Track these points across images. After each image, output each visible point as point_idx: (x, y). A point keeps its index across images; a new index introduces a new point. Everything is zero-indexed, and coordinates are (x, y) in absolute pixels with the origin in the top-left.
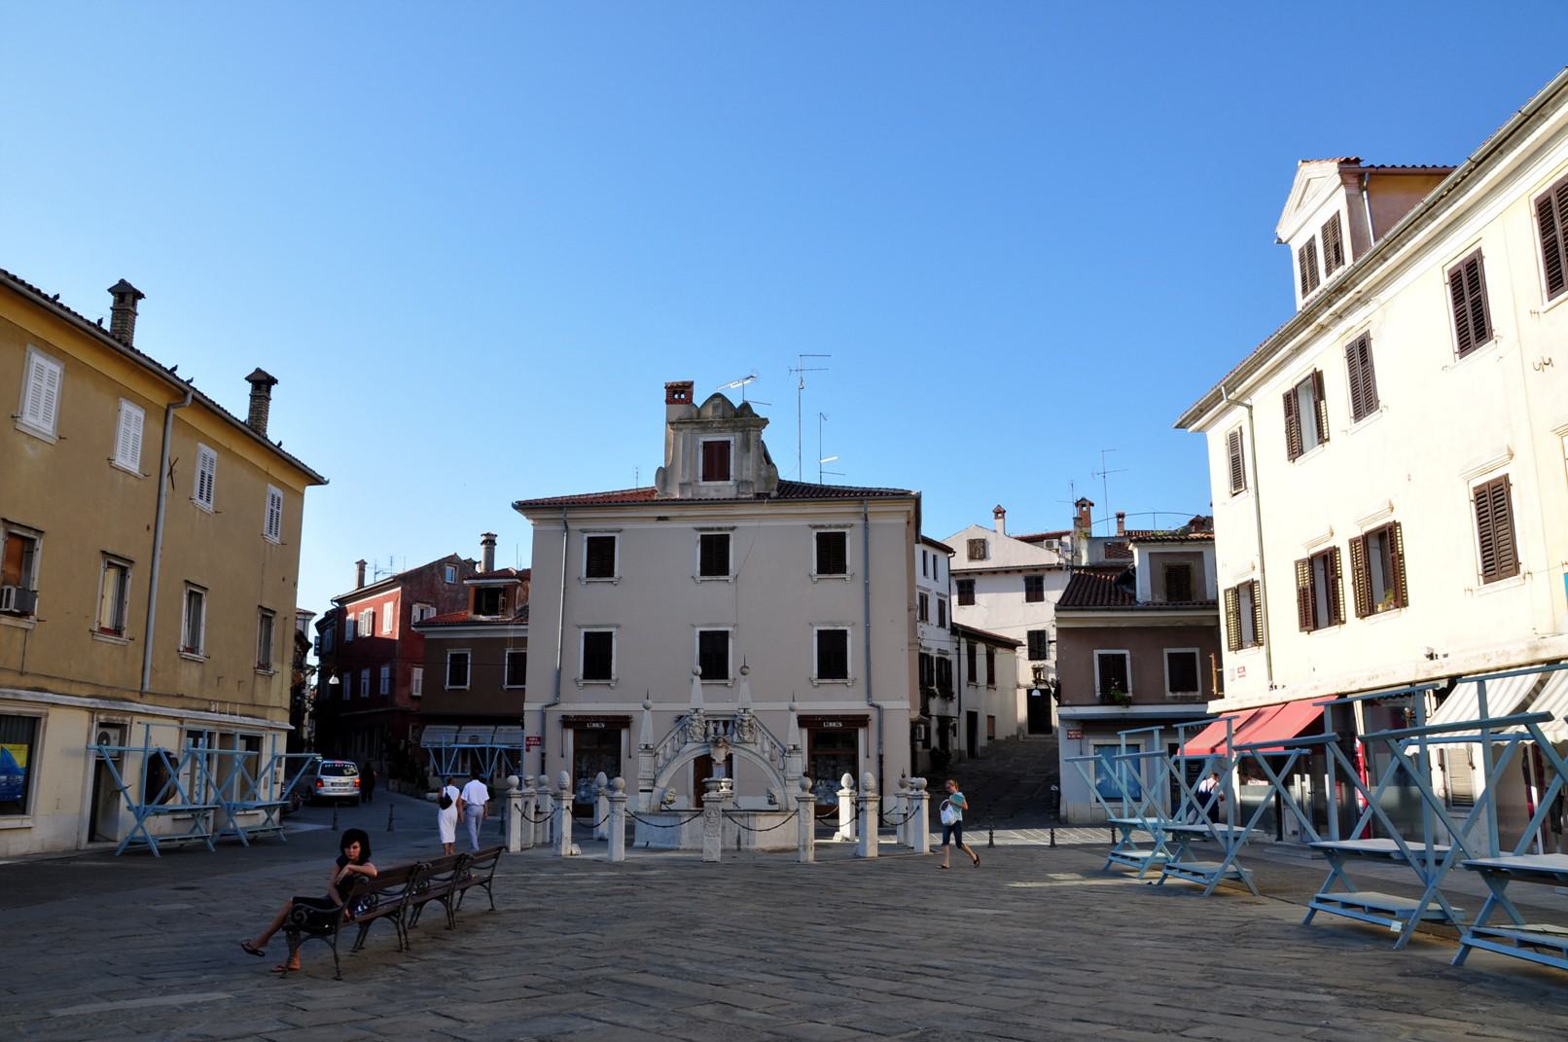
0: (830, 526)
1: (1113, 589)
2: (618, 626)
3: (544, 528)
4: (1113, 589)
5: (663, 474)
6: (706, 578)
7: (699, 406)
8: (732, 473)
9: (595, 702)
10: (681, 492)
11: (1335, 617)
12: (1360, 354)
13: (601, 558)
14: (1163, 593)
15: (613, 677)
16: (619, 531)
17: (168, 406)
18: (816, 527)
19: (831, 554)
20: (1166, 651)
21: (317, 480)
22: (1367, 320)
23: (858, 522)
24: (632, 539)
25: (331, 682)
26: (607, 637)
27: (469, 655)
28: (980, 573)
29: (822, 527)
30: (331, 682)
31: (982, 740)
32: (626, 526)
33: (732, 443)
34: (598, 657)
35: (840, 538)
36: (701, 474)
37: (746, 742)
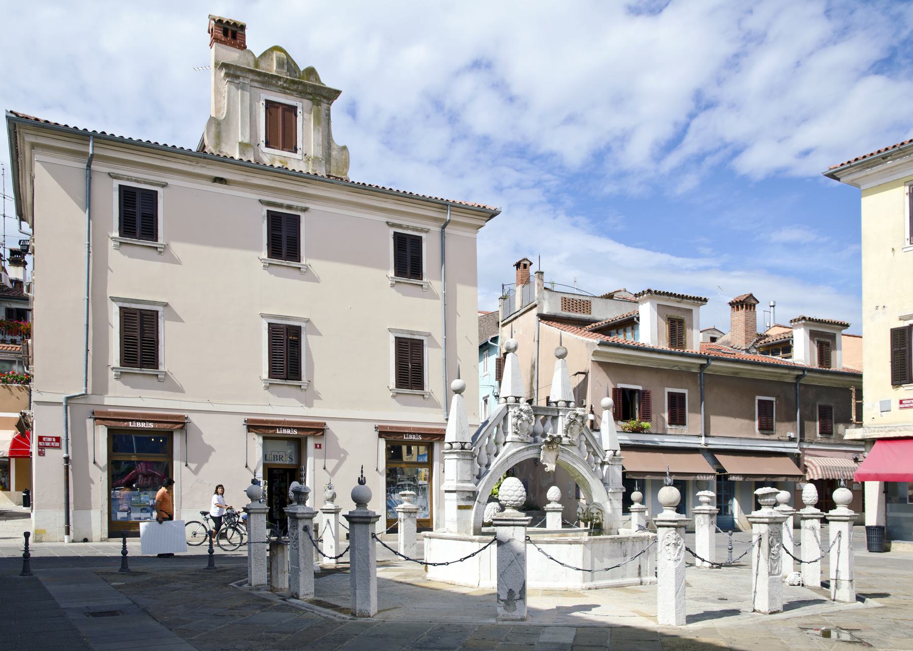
0: (408, 228)
2: (166, 305)
5: (218, 126)
10: (242, 152)
16: (164, 185)
18: (393, 225)
20: (758, 398)
23: (435, 228)
25: (343, 455)
26: (296, 332)
29: (400, 226)
30: (343, 455)
32: (173, 181)
35: (418, 241)
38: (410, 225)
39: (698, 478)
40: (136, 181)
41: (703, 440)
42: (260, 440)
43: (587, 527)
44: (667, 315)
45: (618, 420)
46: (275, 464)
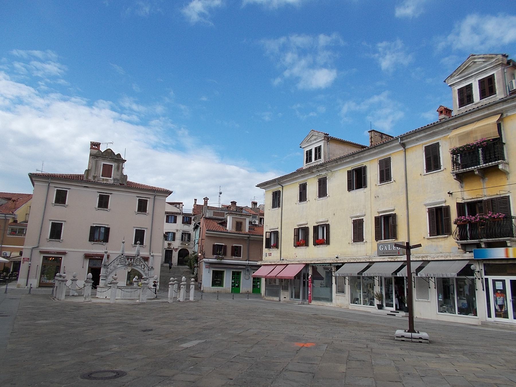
0: (143, 197)
2: (65, 221)
5: (88, 171)
6: (100, 209)
8: (112, 175)
9: (54, 247)
11: (306, 244)
12: (309, 159)
13: (61, 198)
14: (235, 229)
15: (61, 239)
19: (142, 207)
22: (326, 174)
23: (152, 197)
33: (113, 166)
36: (101, 174)
37: (138, 265)
38: (143, 197)
40: (62, 188)
41: (247, 262)
42: (88, 261)
43: (221, 284)
45: (214, 255)
46: (93, 267)
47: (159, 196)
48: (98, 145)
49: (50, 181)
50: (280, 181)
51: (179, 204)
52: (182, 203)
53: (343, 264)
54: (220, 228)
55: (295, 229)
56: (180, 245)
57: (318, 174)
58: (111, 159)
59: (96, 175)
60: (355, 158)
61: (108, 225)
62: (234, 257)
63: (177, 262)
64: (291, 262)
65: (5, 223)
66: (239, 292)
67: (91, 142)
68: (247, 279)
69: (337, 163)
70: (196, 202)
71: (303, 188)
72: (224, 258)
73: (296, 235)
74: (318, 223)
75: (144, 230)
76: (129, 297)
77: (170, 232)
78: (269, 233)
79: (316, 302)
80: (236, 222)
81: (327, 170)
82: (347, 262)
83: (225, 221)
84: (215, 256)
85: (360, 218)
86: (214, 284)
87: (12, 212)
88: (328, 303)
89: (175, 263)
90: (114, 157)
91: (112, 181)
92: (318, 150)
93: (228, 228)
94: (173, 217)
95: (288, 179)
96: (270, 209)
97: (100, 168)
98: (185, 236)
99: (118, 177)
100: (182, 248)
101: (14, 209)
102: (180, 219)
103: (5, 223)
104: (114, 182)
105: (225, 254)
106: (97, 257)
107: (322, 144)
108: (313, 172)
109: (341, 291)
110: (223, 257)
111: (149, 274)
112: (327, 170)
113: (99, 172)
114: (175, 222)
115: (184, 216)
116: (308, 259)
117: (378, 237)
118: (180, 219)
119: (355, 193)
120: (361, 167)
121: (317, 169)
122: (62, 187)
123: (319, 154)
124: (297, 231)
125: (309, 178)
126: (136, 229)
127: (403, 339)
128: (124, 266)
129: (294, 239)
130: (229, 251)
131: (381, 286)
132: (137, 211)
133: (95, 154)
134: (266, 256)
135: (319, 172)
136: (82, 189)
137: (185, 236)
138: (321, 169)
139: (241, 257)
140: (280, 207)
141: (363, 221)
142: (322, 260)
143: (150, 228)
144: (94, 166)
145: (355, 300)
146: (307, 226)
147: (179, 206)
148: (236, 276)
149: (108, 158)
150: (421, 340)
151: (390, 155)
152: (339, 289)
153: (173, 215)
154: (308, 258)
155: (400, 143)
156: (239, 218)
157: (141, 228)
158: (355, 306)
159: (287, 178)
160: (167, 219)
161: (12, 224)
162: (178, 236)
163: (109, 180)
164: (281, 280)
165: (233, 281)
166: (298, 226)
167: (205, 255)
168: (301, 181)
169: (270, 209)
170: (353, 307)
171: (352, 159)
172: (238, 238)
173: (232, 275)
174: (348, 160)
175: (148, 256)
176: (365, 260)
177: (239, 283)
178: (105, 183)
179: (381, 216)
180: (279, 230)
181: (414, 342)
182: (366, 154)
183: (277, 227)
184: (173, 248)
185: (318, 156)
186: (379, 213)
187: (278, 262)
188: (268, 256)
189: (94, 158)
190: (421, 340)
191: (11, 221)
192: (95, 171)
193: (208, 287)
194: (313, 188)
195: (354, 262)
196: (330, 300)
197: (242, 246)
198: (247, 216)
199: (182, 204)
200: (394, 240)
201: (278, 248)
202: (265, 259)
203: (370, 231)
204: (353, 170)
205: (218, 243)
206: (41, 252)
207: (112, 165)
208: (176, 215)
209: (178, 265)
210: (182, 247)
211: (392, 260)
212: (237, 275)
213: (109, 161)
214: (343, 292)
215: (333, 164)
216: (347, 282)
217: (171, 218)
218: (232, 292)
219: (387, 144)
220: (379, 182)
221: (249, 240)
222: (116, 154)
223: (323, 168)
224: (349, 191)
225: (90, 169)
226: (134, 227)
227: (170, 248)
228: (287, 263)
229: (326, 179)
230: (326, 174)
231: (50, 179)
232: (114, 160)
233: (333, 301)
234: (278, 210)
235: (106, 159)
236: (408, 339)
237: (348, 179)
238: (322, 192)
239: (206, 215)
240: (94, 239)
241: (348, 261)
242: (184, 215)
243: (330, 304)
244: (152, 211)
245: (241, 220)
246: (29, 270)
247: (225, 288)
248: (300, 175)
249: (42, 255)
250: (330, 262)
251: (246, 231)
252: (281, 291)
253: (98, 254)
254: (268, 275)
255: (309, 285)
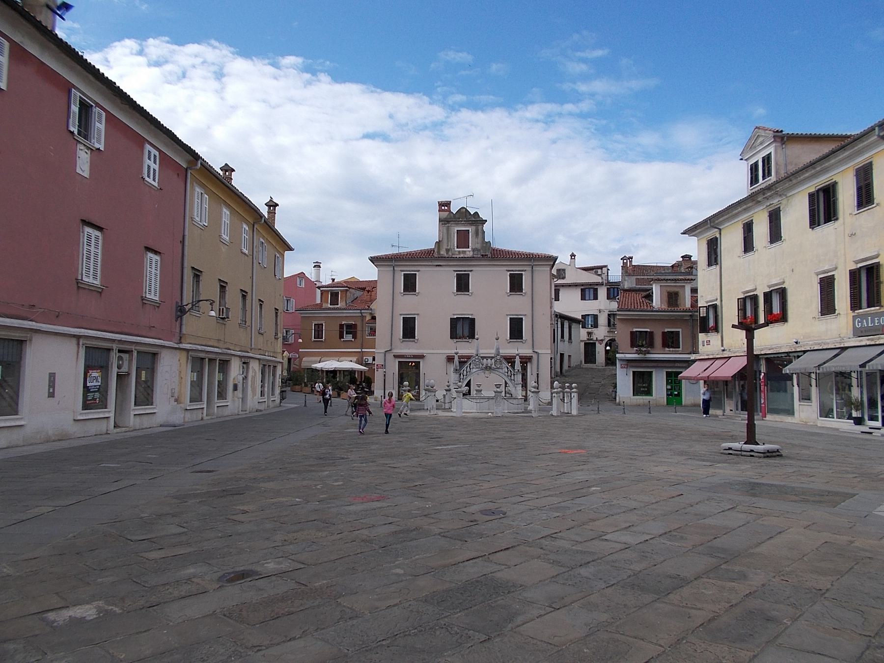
0: (516, 271)
1: (641, 301)
2: (418, 314)
3: (379, 269)
4: (641, 301)
5: (438, 244)
6: (459, 293)
7: (454, 213)
9: (408, 349)
12: (754, 180)
13: (410, 284)
16: (418, 271)
17: (254, 223)
19: (516, 284)
21: (291, 249)
22: (779, 202)
23: (529, 269)
24: (425, 276)
27: (324, 325)
28: (563, 286)
29: (512, 271)
31: (565, 367)
33: (470, 231)
34: (409, 329)
36: (456, 245)
37: (498, 368)
38: (516, 270)
39: (723, 392)
40: (409, 271)
43: (649, 392)
44: (667, 290)
47: (538, 266)
48: (448, 204)
49: (393, 263)
50: (714, 222)
51: (601, 268)
52: (606, 266)
53: (805, 352)
54: (642, 305)
55: (738, 299)
56: (607, 334)
57: (769, 204)
58: (466, 221)
59: (449, 248)
60: (818, 169)
61: (472, 315)
62: (668, 349)
63: (604, 362)
64: (734, 353)
65: (362, 320)
66: (680, 403)
67: (439, 202)
68: (693, 384)
69: (791, 182)
70: (632, 260)
71: (748, 228)
72: (651, 352)
73: (741, 309)
74: (771, 287)
75: (522, 318)
76: (486, 410)
77: (588, 315)
78: (705, 308)
79: (773, 416)
80: (668, 292)
81: (778, 194)
82: (809, 349)
83: (650, 293)
84: (635, 349)
85: (830, 274)
86: (636, 392)
87: (368, 306)
88: (789, 418)
89: (602, 363)
90: (470, 218)
91: (471, 252)
92: (767, 160)
93: (654, 304)
94: (592, 290)
95: (726, 217)
96: (705, 268)
97: (454, 236)
98: (614, 320)
99: (478, 246)
100: (611, 338)
101: (370, 301)
102: (602, 292)
103: (362, 320)
104: (473, 254)
105: (651, 345)
106: (463, 360)
107: (771, 150)
108: (760, 202)
109: (806, 397)
110: (649, 351)
111: (515, 380)
112: (780, 196)
113: (452, 242)
114: (596, 298)
115: (608, 287)
116: (758, 347)
117: (855, 304)
118: (602, 292)
119: (822, 232)
120: (829, 185)
121: (764, 195)
122: (410, 270)
123: (769, 167)
124: (742, 303)
125: (756, 211)
126: (510, 318)
127: (730, 452)
128: (480, 370)
129: (738, 316)
130: (658, 340)
131: (862, 387)
132: (509, 292)
133: (445, 218)
134: (704, 346)
135: (768, 199)
136: (433, 269)
137: (614, 320)
138: (769, 194)
139: (681, 349)
140: (717, 264)
141: (834, 279)
142: (776, 349)
143: (529, 313)
144: (446, 235)
145: (826, 412)
146: (755, 293)
147: (602, 272)
148: (673, 378)
149: (462, 221)
150: (752, 454)
151: (872, 157)
152: (804, 394)
153: (592, 287)
154: (759, 345)
155: (879, 136)
156: (672, 286)
157: (517, 315)
158: (826, 420)
159: (723, 216)
160: (583, 294)
161: (370, 322)
162: (603, 320)
163: (467, 252)
164: (360, 373)
165: (669, 387)
166: (744, 294)
167: (619, 348)
168: (744, 217)
169: (705, 268)
170: (823, 422)
171: (813, 171)
172: (673, 318)
173: (667, 377)
174: (807, 175)
175: (531, 355)
176: (834, 344)
177: (679, 389)
178: (462, 257)
179: (860, 267)
180: (718, 302)
181: (745, 456)
182: (833, 161)
183: (715, 298)
184: (595, 339)
185: (766, 171)
186: (857, 262)
187: (718, 354)
188: (705, 345)
189: (445, 224)
190: (752, 454)
191: (368, 318)
192: (448, 243)
193: (627, 397)
194: (761, 230)
195: (818, 348)
196: (790, 412)
197: (680, 330)
198: (686, 281)
199: (605, 268)
200: (878, 308)
201: (719, 332)
202: (702, 351)
203: (844, 295)
204: (818, 191)
205: (638, 328)
206: (396, 356)
207: (469, 230)
208: (596, 287)
209: (606, 366)
210: (610, 337)
211: (873, 343)
212: (675, 377)
213: (464, 225)
214: (809, 400)
215: (785, 184)
216: (813, 382)
217: (589, 292)
218: (667, 405)
219: (861, 140)
220: (856, 208)
221: (693, 320)
222: (472, 214)
223: (773, 192)
224: (813, 228)
225: (441, 240)
226: (507, 315)
227: (592, 340)
228: (730, 356)
229: (780, 211)
230: (779, 202)
231: (394, 261)
232: (470, 222)
233: (795, 414)
234: (715, 269)
235: (460, 222)
236: (736, 452)
237: (811, 208)
238: (775, 235)
239: (624, 286)
240: (456, 336)
241: (811, 348)
242: (609, 286)
243: (792, 419)
244: (530, 290)
245: (676, 290)
246: (385, 379)
247: (655, 398)
248: (741, 208)
249: (397, 360)
250: (787, 351)
251: (687, 306)
252: (726, 399)
253: (463, 355)
254: (699, 376)
255: (762, 389)
